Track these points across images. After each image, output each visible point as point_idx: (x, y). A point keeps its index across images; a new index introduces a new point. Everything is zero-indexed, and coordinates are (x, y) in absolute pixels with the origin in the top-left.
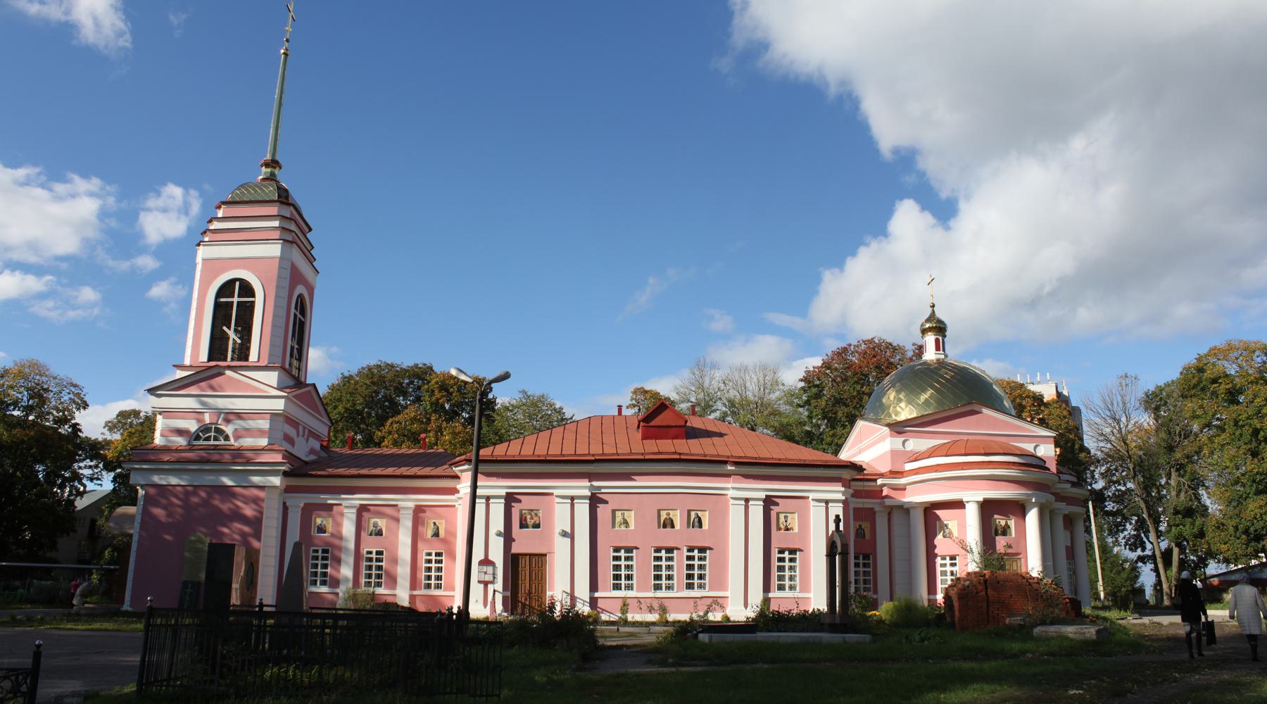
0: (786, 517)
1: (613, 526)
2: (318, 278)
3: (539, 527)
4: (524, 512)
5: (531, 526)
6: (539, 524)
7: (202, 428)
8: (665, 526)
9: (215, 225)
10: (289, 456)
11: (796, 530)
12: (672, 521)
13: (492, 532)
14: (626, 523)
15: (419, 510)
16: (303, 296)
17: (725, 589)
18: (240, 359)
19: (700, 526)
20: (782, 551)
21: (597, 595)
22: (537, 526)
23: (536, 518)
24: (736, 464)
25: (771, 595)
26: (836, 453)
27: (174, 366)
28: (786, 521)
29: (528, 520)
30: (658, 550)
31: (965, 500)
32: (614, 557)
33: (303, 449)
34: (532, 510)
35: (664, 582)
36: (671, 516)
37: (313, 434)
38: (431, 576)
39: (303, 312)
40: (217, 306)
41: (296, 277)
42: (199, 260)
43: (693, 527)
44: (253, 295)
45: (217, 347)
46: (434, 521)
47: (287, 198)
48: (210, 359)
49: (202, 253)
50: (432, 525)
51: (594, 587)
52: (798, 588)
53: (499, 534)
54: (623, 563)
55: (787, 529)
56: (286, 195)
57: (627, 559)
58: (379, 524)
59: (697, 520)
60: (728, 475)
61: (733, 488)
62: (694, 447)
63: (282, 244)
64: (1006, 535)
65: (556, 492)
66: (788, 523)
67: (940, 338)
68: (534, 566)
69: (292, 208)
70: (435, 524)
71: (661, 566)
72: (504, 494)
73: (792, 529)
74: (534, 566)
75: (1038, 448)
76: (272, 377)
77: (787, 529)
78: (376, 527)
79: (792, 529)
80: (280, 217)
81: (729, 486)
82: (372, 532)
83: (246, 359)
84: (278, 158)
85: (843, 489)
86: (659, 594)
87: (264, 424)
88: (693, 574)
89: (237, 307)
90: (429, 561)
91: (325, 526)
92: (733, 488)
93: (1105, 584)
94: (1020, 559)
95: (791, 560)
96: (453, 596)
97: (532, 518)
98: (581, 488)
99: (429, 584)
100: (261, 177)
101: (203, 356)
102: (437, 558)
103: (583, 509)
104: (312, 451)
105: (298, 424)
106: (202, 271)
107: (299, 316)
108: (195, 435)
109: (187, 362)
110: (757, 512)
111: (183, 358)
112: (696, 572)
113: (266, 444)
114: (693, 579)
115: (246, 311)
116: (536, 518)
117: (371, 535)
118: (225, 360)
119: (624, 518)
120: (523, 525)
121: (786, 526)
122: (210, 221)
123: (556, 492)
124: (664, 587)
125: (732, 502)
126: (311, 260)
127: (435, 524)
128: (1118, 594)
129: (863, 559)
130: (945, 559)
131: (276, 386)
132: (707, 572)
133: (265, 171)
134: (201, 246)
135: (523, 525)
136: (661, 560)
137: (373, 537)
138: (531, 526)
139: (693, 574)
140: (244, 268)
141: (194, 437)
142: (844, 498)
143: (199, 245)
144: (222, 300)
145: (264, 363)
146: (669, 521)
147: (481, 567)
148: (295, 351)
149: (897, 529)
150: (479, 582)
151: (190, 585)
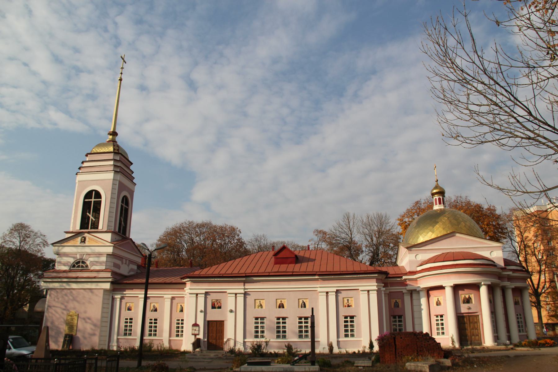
0: (348, 300)
1: (255, 308)
2: (136, 186)
4: (213, 301)
5: (217, 307)
7: (76, 262)
8: (279, 307)
9: (85, 164)
10: (114, 273)
11: (353, 306)
12: (283, 305)
14: (261, 306)
15: (173, 298)
16: (127, 197)
17: (361, 337)
18: (94, 228)
19: (305, 307)
20: (346, 317)
21: (246, 340)
23: (219, 304)
24: (319, 275)
25: (340, 340)
27: (65, 232)
28: (348, 302)
29: (216, 305)
30: (278, 319)
32: (299, 322)
33: (125, 270)
34: (217, 300)
35: (349, 333)
36: (282, 302)
37: (132, 262)
38: (258, 331)
39: (127, 204)
40: (85, 203)
41: (121, 187)
42: (77, 181)
44: (100, 198)
45: (84, 224)
46: (181, 304)
47: (118, 150)
48: (81, 228)
49: (80, 178)
50: (180, 306)
51: (338, 337)
52: (355, 336)
53: (201, 312)
54: (259, 325)
55: (349, 306)
56: (118, 148)
57: (283, 323)
58: (156, 306)
59: (303, 304)
60: (317, 280)
61: (320, 287)
62: (297, 268)
63: (114, 173)
65: (228, 291)
66: (349, 303)
69: (120, 155)
70: (181, 305)
71: (302, 326)
72: (204, 293)
76: (108, 237)
77: (349, 306)
79: (351, 306)
83: (97, 228)
84: (117, 131)
85: (376, 284)
86: (258, 340)
87: (104, 259)
89: (94, 203)
90: (179, 324)
91: (131, 307)
92: (320, 287)
95: (262, 323)
96: (182, 340)
97: (217, 304)
98: (239, 288)
99: (257, 335)
100: (108, 140)
101: (78, 227)
103: (240, 299)
104: (132, 270)
105: (123, 258)
106: (78, 187)
107: (124, 205)
108: (73, 265)
109: (71, 230)
110: (332, 298)
111: (69, 228)
112: (303, 329)
115: (98, 205)
117: (152, 311)
118: (88, 229)
119: (260, 304)
120: (213, 307)
121: (348, 305)
122: (83, 163)
123: (228, 291)
125: (361, 292)
126: (131, 179)
127: (181, 305)
129: (398, 318)
131: (110, 241)
132: (355, 328)
133: (111, 137)
134: (78, 175)
135: (213, 307)
136: (282, 322)
138: (217, 307)
139: (348, 330)
140: (97, 185)
141: (72, 266)
142: (377, 289)
143: (77, 174)
144: (86, 200)
145: (105, 229)
146: (281, 305)
147: (193, 327)
148: (123, 223)
150: (192, 334)
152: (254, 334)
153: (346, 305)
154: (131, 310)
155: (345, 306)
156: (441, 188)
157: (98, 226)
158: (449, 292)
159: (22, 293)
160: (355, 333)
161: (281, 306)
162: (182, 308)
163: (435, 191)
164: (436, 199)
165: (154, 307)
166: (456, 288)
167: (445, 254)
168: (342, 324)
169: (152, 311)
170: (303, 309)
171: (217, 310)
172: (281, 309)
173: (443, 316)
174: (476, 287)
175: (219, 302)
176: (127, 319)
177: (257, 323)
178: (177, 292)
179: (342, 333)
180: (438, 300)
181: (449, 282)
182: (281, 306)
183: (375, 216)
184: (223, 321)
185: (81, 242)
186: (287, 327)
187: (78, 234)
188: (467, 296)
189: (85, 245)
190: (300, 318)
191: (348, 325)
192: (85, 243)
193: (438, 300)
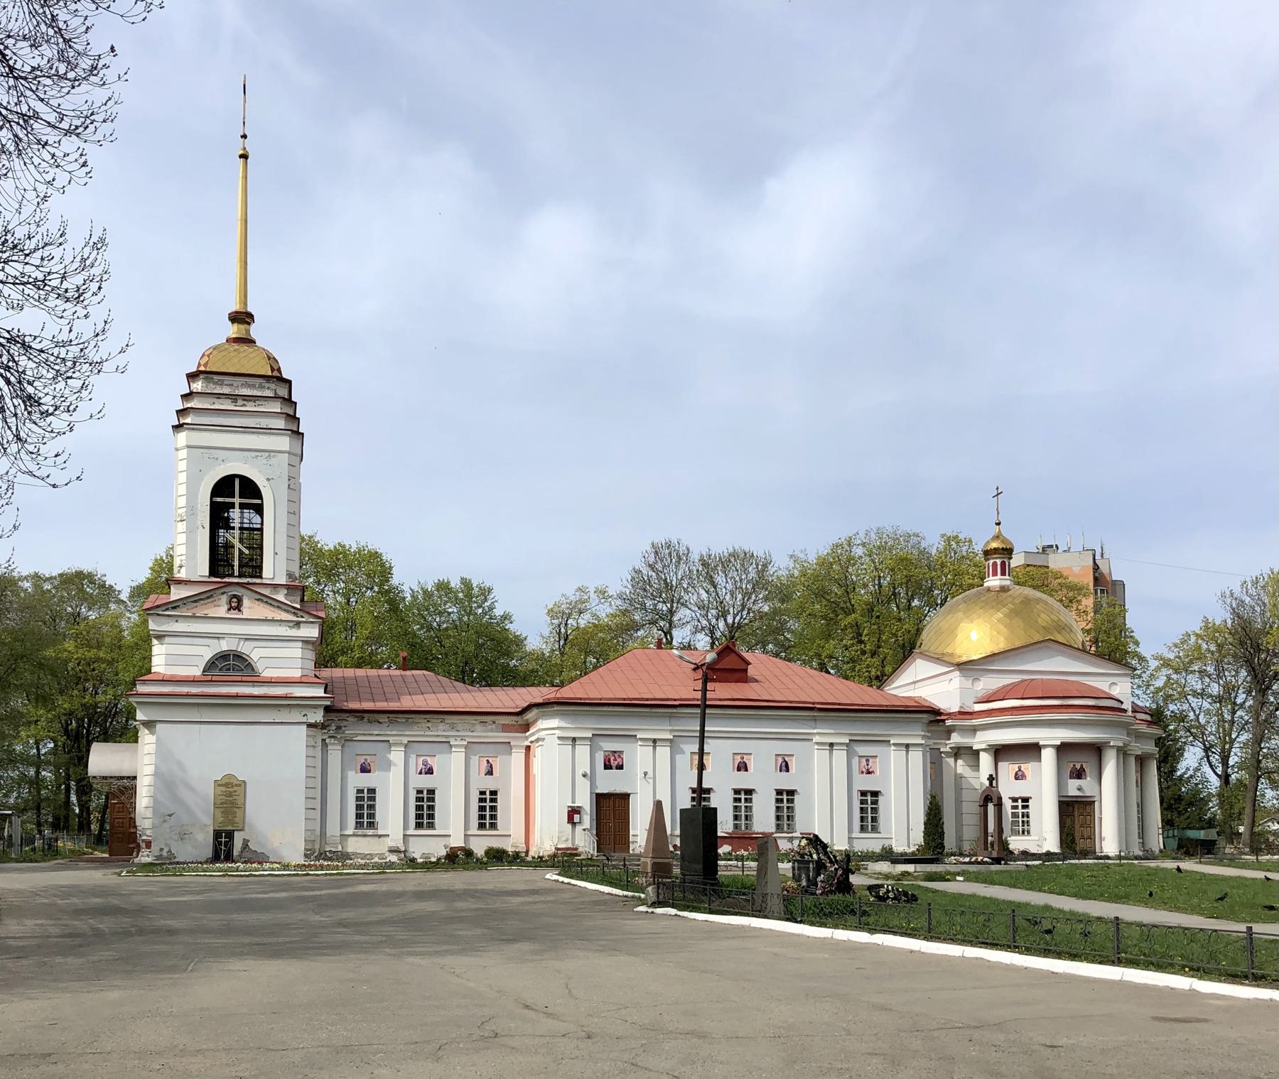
0: (867, 761)
3: (622, 769)
5: (614, 767)
6: (622, 765)
8: (739, 769)
12: (746, 764)
13: (579, 773)
19: (787, 770)
20: (863, 793)
22: (620, 767)
23: (619, 760)
26: (881, 680)
28: (868, 765)
29: (612, 761)
31: (1041, 743)
34: (615, 752)
40: (214, 507)
43: (781, 771)
55: (869, 772)
57: (1024, 807)
59: (784, 764)
64: (1081, 779)
67: (1006, 561)
68: (617, 806)
70: (488, 761)
73: (873, 772)
74: (617, 806)
75: (1115, 686)
78: (425, 765)
79: (873, 772)
80: (284, 416)
81: (815, 731)
82: (421, 770)
88: (485, 807)
90: (362, 799)
93: (797, 913)
94: (1094, 802)
97: (615, 760)
102: (484, 797)
113: (300, 675)
114: (485, 811)
116: (619, 760)
117: (420, 773)
120: (607, 766)
121: (868, 769)
124: (425, 826)
127: (488, 761)
128: (507, 622)
130: (740, 794)
135: (607, 766)
137: (423, 776)
149: (811, 718)
151: (224, 834)
152: (1011, 819)
153: (864, 770)
154: (369, 771)
155: (862, 772)
156: (1005, 540)
157: (260, 567)
158: (1048, 756)
159: (86, 719)
160: (437, 821)
161: (743, 767)
162: (491, 766)
163: (994, 545)
164: (995, 564)
165: (425, 763)
166: (1064, 749)
167: (1027, 683)
168: (475, 805)
169: (420, 773)
170: (784, 773)
171: (614, 771)
172: (742, 773)
173: (1030, 800)
174: (1097, 750)
175: (619, 756)
176: (482, 793)
177: (739, 800)
178: (658, 725)
179: (474, 821)
180: (1020, 770)
181: (1051, 737)
182: (743, 767)
183: (652, 560)
184: (625, 797)
185: (229, 610)
186: (498, 807)
187: (225, 586)
188: (1078, 766)
189: (240, 616)
190: (737, 792)
191: (741, 806)
192: (239, 610)
193: (1020, 770)
